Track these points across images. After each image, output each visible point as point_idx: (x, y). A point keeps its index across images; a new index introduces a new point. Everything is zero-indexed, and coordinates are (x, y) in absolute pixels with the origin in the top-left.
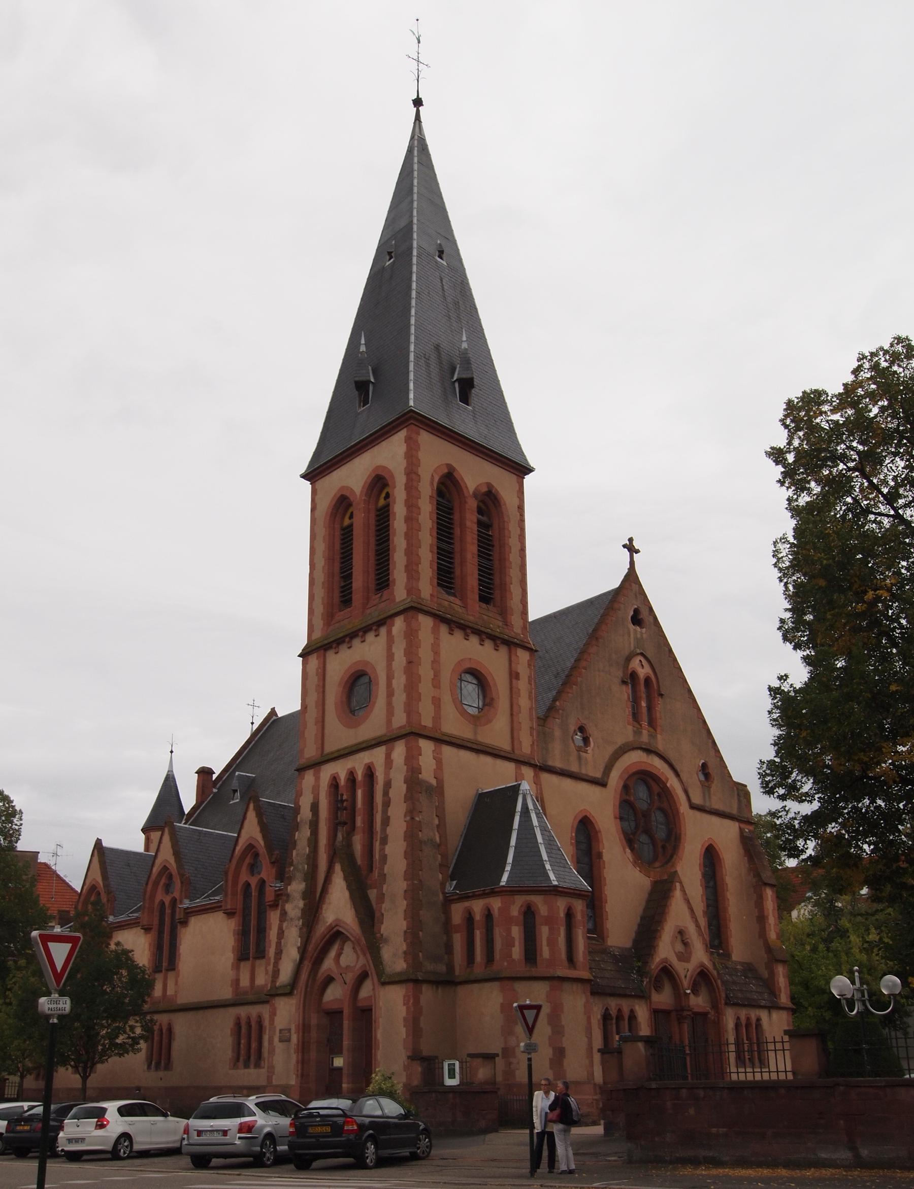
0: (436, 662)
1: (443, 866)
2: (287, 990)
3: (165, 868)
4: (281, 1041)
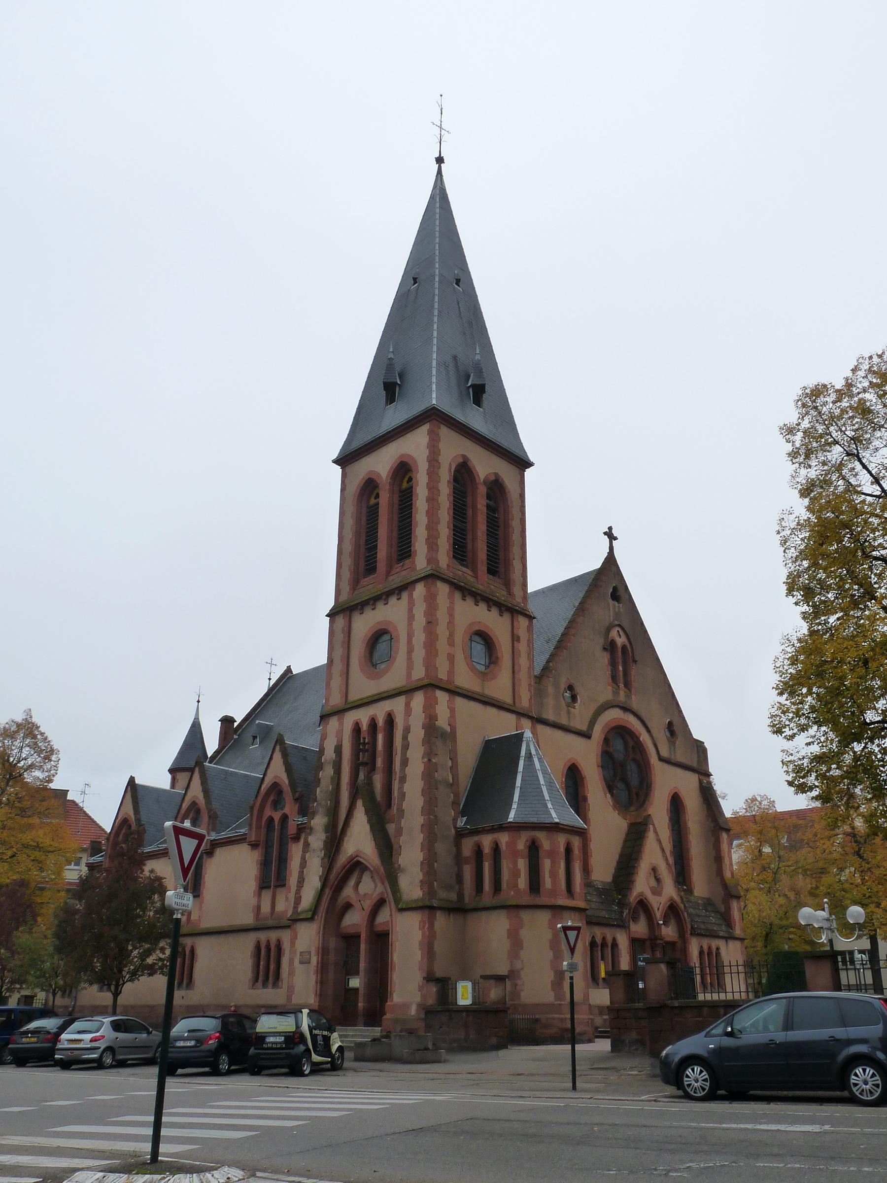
0: (451, 623)
1: (455, 803)
2: (309, 915)
3: (194, 804)
4: (301, 962)
